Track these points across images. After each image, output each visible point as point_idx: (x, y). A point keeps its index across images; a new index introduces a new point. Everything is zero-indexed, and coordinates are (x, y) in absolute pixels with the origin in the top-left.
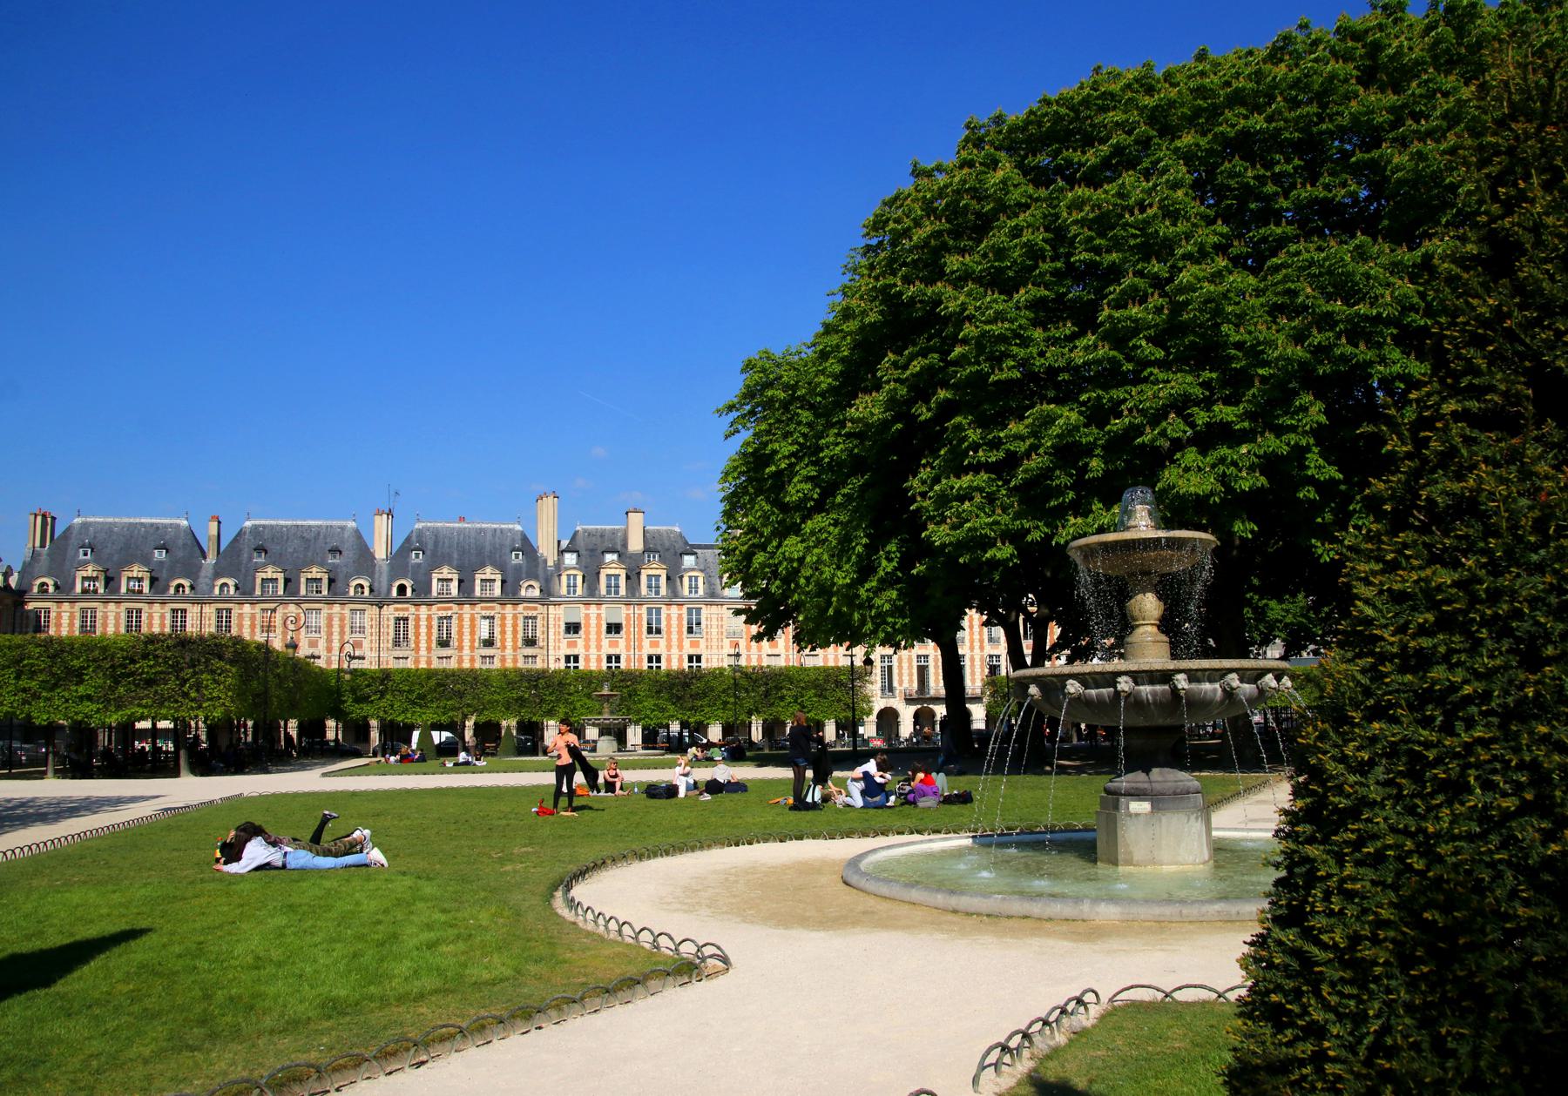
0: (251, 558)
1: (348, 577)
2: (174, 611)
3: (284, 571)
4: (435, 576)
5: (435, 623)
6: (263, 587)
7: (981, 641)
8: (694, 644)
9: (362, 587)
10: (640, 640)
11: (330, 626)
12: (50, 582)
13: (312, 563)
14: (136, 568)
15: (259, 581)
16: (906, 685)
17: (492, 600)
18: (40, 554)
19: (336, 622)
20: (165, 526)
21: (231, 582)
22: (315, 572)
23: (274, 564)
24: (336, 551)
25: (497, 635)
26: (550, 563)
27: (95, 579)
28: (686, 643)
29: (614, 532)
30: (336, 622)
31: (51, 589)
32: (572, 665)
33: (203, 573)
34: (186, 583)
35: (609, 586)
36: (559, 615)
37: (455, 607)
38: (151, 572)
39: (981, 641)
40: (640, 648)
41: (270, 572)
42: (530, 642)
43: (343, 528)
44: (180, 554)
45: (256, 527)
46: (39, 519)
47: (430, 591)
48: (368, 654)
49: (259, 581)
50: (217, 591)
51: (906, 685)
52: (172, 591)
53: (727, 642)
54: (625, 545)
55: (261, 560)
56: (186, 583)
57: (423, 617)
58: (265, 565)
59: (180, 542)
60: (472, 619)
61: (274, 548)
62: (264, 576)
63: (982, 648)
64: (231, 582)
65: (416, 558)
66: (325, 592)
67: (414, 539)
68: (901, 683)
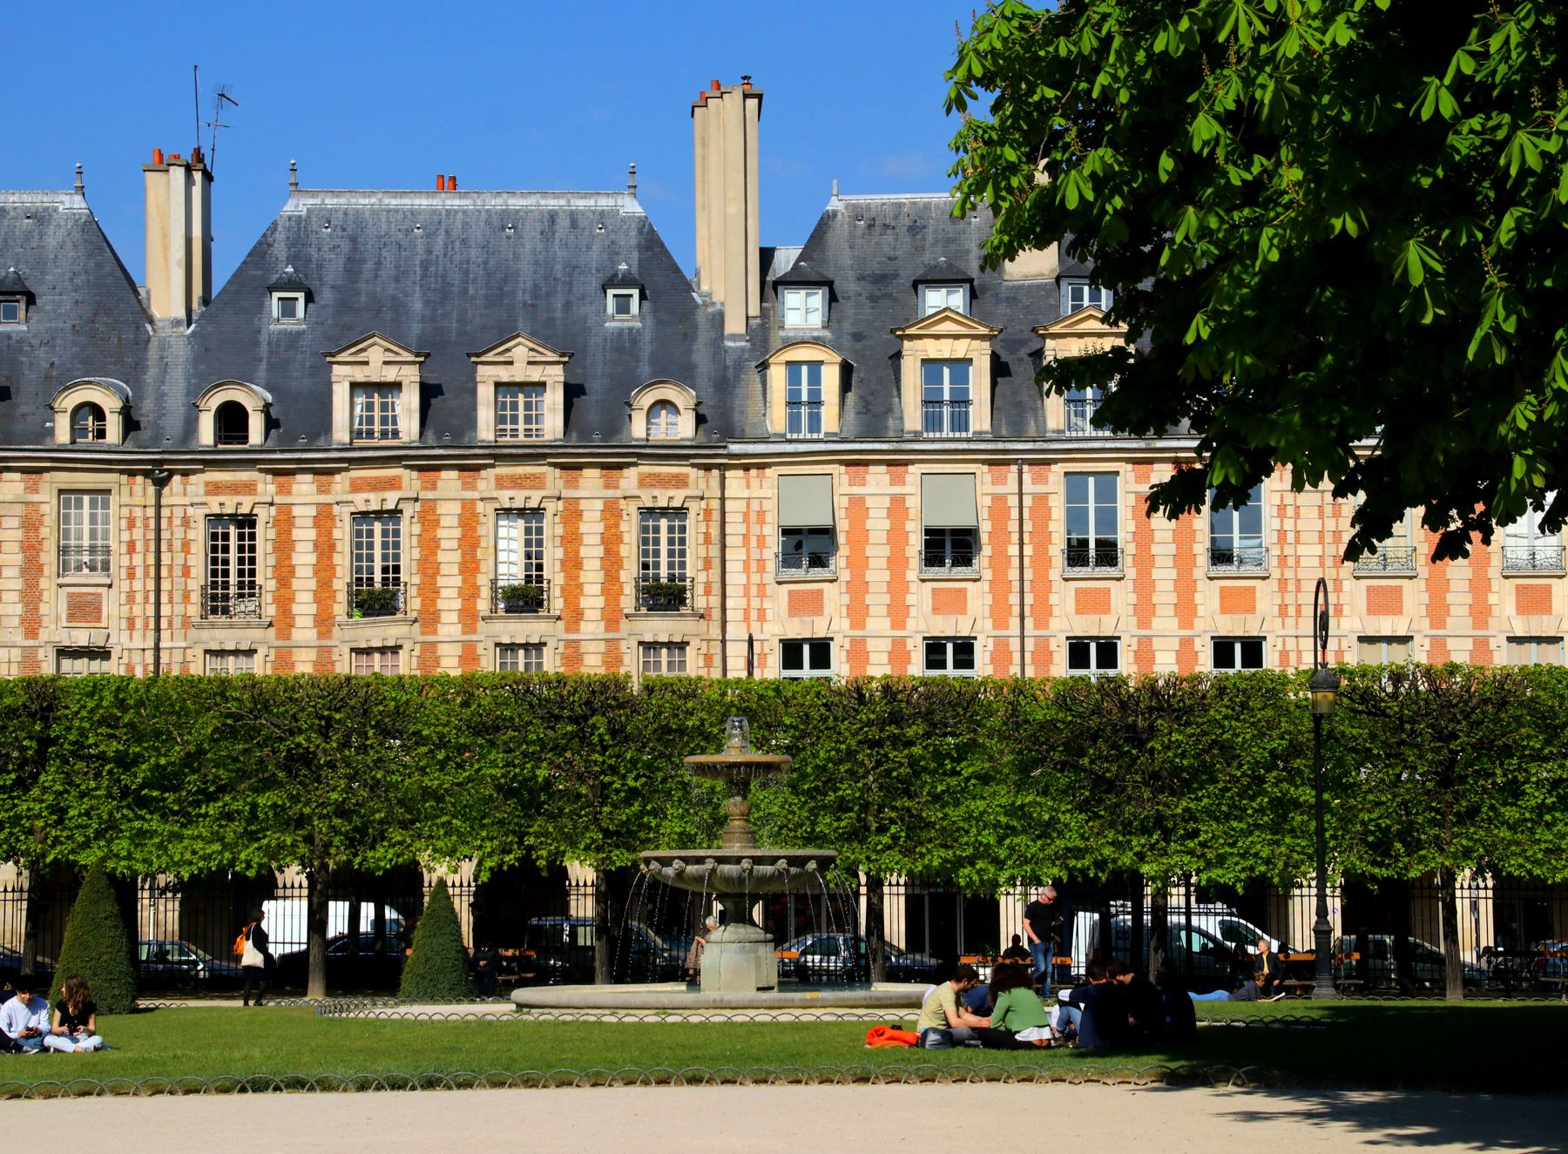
4: (342, 376)
6: (499, 406)
8: (1235, 602)
9: (98, 413)
17: (536, 455)
25: (553, 574)
26: (735, 325)
35: (793, 402)
36: (759, 502)
37: (410, 481)
42: (665, 596)
43: (41, 218)
47: (326, 426)
48: (119, 640)
57: (304, 514)
60: (469, 520)
67: (280, 250)
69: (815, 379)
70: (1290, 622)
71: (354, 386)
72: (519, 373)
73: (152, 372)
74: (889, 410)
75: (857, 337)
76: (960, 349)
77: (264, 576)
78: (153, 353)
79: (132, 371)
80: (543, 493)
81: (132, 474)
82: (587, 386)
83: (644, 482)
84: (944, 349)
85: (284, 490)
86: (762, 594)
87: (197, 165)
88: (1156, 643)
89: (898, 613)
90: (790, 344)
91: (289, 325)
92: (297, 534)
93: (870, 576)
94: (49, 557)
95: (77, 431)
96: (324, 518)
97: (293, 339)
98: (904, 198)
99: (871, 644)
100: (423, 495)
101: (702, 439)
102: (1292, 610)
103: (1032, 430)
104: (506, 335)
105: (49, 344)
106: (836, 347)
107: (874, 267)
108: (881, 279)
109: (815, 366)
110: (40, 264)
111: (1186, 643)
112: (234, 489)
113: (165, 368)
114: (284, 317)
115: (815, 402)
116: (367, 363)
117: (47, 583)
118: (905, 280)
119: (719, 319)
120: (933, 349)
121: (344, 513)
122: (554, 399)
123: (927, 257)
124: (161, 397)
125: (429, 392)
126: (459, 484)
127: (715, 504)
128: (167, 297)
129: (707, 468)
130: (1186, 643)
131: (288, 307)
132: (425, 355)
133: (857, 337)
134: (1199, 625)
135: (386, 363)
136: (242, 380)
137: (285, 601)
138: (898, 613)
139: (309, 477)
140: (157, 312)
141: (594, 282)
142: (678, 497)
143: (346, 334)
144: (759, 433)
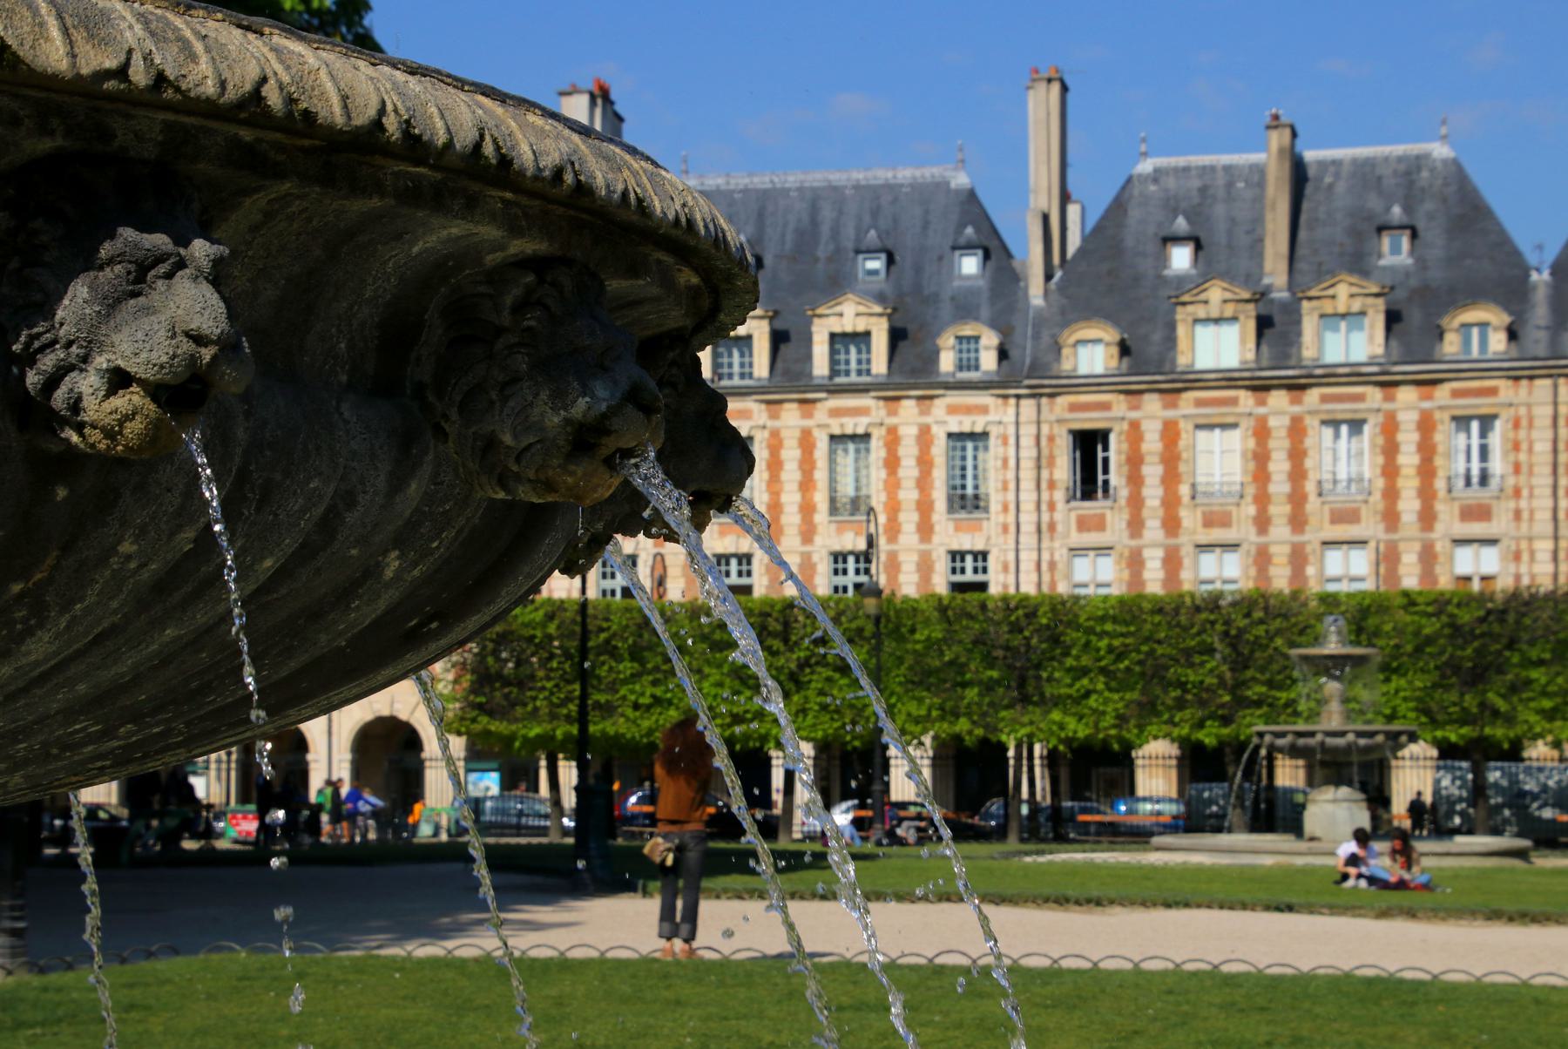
5: (822, 445)
6: (833, 352)
7: (924, 507)
37: (1374, 395)
39: (807, 509)
57: (909, 432)
60: (1426, 425)
63: (925, 529)
70: (1524, 526)
77: (1116, 478)
80: (751, 423)
81: (1517, 379)
82: (1405, 313)
83: (1325, 399)
85: (1262, 403)
88: (1402, 546)
92: (1401, 437)
93: (784, 498)
96: (924, 436)
100: (769, 423)
101: (1514, 354)
102: (1525, 515)
103: (1167, 368)
112: (969, 410)
116: (1206, 302)
121: (939, 433)
125: (897, 336)
126: (916, 411)
127: (1011, 430)
129: (1005, 397)
135: (858, 315)
139: (1155, 396)
141: (1152, 247)
142: (1483, 405)
144: (1054, 373)
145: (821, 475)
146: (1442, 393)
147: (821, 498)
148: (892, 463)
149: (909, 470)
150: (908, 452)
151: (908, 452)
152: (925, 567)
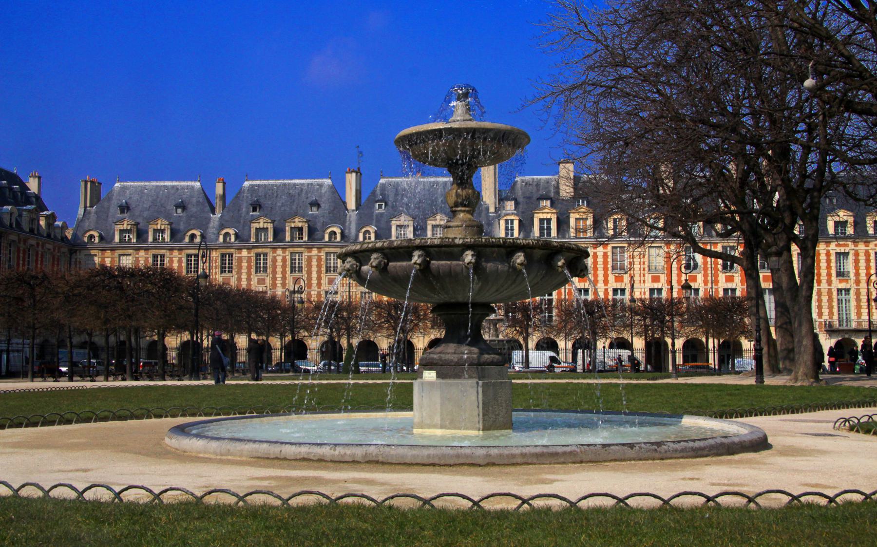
0: (248, 213)
1: (325, 226)
2: (189, 256)
3: (273, 222)
4: (394, 223)
5: (833, 258)
6: (433, 230)
7: (829, 275)
9: (334, 233)
10: (717, 276)
11: (309, 266)
12: (96, 234)
13: (295, 214)
14: (438, 217)
15: (253, 231)
16: (825, 317)
17: (846, 238)
18: (90, 213)
19: (314, 263)
20: (183, 188)
21: (232, 231)
22: (298, 222)
23: (266, 216)
24: (316, 204)
26: (492, 210)
27: (129, 231)
28: (611, 278)
29: (548, 182)
30: (314, 263)
31: (97, 240)
32: (619, 297)
33: (211, 224)
34: (197, 233)
35: (507, 229)
38: (170, 224)
39: (829, 275)
40: (716, 282)
41: (261, 224)
43: (321, 185)
44: (194, 210)
45: (252, 186)
46: (89, 184)
47: (390, 236)
49: (253, 231)
50: (221, 239)
51: (825, 317)
52: (187, 239)
53: (648, 277)
54: (557, 191)
55: (257, 213)
56: (197, 233)
58: (259, 218)
59: (194, 200)
61: (267, 203)
62: (434, 223)
63: (829, 282)
64: (232, 231)
65: (379, 209)
66: (306, 238)
67: (378, 192)
68: (820, 314)
69: (512, 223)
71: (397, 226)
72: (401, 223)
73: (347, 224)
74: (531, 231)
75: (523, 212)
76: (549, 216)
78: (348, 218)
79: (343, 223)
84: (544, 216)
86: (644, 276)
87: (358, 172)
89: (606, 282)
90: (506, 215)
91: (381, 211)
94: (610, 266)
95: (330, 238)
97: (382, 214)
98: (535, 177)
99: (823, 290)
104: (435, 214)
105: (323, 216)
106: (517, 215)
107: (527, 195)
108: (529, 198)
109: (512, 221)
110: (321, 197)
111: (606, 290)
113: (350, 222)
114: (379, 209)
115: (512, 229)
117: (609, 272)
118: (535, 198)
119: (488, 209)
120: (542, 216)
121: (833, 253)
122: (411, 229)
123: (540, 193)
124: (350, 229)
128: (351, 204)
130: (606, 290)
131: (380, 207)
132: (414, 218)
133: (523, 212)
134: (609, 285)
136: (369, 224)
137: (596, 275)
138: (606, 282)
140: (349, 207)
143: (395, 214)
145: (833, 264)
146: (833, 246)
147: (834, 272)
148: (857, 261)
149: (862, 264)
150: (862, 258)
151: (862, 258)
152: (606, 292)
